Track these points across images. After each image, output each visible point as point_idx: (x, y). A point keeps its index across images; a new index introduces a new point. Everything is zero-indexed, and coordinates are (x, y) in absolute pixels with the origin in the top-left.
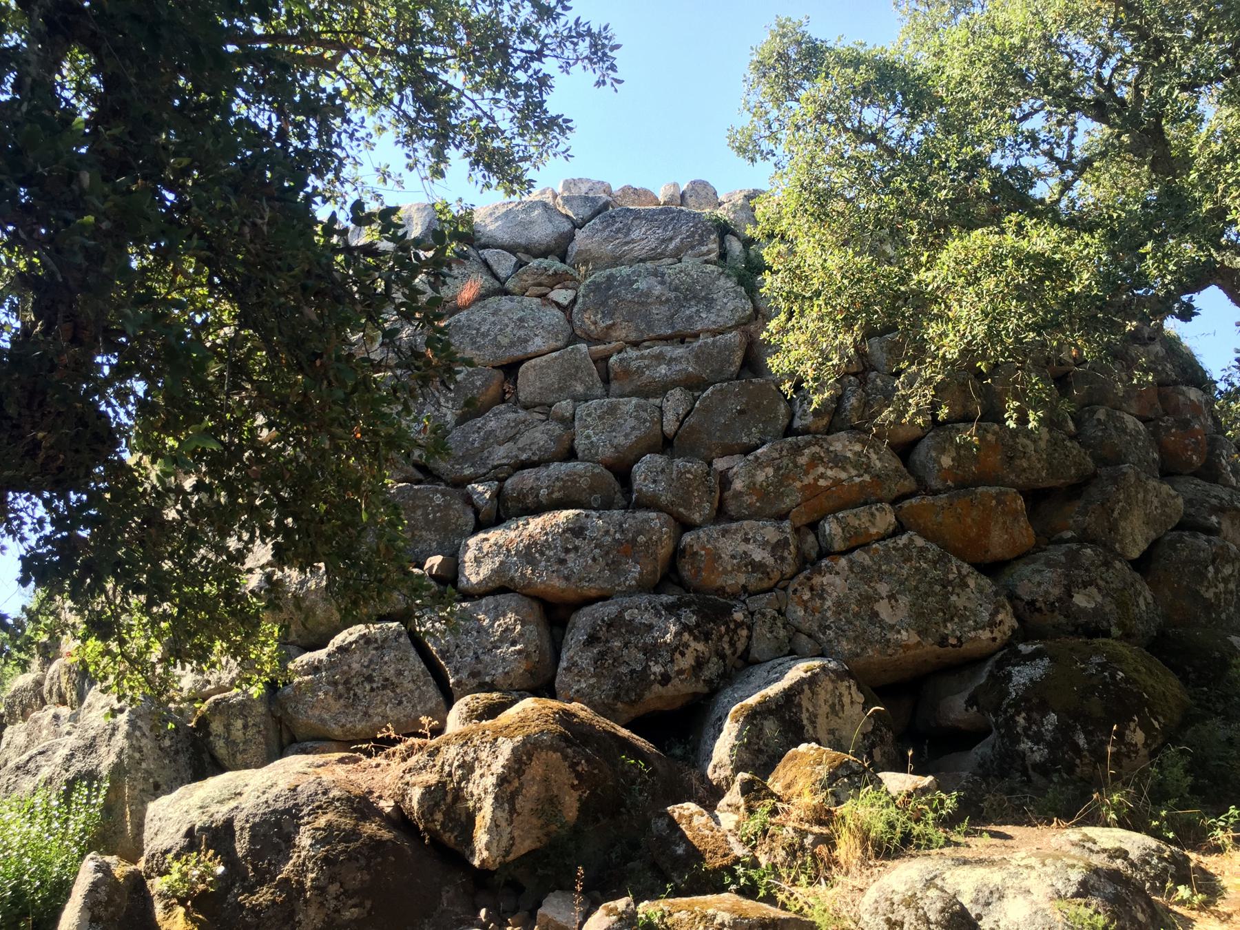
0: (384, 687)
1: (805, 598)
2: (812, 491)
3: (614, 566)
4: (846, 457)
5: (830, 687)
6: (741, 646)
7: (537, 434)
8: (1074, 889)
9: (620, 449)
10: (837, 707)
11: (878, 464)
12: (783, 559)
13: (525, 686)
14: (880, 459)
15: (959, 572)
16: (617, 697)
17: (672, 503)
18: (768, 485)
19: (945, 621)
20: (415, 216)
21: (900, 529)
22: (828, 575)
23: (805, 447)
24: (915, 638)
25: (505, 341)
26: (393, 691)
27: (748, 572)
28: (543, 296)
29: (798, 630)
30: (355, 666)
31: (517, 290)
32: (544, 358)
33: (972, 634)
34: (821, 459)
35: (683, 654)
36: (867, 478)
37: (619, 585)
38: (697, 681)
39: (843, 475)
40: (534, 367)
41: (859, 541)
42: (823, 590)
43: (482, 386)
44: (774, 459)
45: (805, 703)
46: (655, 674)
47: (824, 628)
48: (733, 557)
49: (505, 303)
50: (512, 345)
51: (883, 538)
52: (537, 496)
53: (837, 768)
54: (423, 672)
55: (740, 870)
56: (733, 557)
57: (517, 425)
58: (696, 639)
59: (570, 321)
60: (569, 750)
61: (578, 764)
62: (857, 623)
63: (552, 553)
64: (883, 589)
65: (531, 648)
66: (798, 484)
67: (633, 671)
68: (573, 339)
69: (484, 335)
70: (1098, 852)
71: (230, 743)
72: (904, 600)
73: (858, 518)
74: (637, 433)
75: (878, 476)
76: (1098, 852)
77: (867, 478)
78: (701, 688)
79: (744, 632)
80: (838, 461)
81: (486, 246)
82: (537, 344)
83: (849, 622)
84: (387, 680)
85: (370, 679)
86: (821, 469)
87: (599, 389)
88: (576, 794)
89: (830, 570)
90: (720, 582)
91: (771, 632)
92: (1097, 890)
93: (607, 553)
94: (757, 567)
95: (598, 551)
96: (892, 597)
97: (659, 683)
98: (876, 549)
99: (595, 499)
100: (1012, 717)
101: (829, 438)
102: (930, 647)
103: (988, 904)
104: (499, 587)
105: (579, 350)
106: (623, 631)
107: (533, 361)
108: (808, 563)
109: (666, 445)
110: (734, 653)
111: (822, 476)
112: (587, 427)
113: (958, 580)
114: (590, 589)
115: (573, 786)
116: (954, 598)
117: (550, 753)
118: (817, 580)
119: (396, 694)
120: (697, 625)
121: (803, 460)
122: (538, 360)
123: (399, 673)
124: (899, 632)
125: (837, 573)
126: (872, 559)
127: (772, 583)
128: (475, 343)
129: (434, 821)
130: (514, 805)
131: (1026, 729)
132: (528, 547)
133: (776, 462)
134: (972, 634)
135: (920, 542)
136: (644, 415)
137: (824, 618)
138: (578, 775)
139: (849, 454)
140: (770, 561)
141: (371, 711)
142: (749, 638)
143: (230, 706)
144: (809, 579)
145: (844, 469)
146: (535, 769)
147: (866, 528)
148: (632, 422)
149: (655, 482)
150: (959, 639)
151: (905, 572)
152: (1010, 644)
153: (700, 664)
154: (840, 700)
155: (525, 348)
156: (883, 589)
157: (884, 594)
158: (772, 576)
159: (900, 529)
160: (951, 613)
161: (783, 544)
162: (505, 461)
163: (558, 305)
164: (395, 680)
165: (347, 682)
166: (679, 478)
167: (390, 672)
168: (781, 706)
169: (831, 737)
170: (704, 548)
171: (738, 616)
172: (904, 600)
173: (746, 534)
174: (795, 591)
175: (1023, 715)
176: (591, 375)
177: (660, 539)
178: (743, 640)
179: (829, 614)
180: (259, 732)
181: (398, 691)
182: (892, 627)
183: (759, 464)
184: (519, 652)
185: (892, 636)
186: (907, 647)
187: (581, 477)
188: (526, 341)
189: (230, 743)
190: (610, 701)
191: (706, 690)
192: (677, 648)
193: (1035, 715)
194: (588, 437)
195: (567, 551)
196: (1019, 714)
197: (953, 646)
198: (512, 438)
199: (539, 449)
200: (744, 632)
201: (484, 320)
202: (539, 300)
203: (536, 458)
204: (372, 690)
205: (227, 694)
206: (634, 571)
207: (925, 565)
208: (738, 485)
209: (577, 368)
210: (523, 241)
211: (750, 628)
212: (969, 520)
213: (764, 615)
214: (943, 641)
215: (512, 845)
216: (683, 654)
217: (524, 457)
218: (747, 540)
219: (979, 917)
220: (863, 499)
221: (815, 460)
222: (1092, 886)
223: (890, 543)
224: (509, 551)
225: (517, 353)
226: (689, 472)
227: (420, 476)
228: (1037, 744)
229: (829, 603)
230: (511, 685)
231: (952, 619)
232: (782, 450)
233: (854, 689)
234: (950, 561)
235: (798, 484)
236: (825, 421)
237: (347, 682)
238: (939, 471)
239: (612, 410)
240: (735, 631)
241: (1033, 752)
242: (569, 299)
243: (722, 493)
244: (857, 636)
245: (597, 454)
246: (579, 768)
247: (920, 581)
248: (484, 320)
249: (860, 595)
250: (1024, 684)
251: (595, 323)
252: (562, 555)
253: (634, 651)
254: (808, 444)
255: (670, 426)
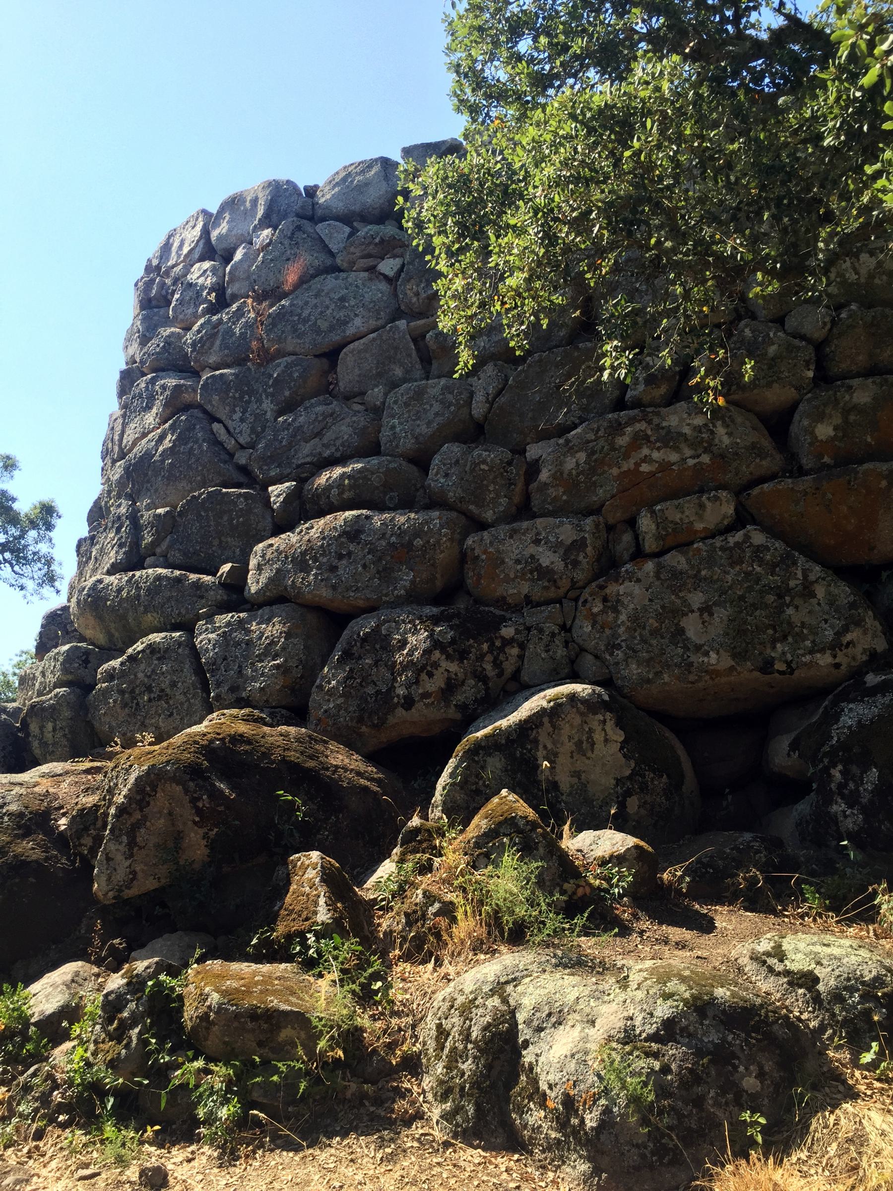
0: (160, 698)
1: (595, 610)
2: (633, 478)
3: (386, 575)
4: (680, 434)
5: (578, 720)
6: (509, 667)
7: (343, 428)
8: (651, 1030)
9: (421, 439)
10: (585, 745)
11: (726, 440)
12: (576, 563)
13: (284, 703)
14: (729, 434)
15: (805, 576)
16: (360, 720)
17: (461, 500)
18: (578, 475)
19: (774, 642)
20: (260, 195)
21: (741, 519)
22: (627, 583)
23: (628, 424)
24: (727, 662)
25: (324, 325)
26: (167, 703)
27: (532, 580)
28: (372, 269)
29: (583, 650)
30: (140, 675)
31: (345, 265)
32: (362, 341)
33: (808, 658)
34: (647, 438)
35: (430, 675)
36: (706, 459)
37: (386, 595)
38: (447, 706)
39: (674, 457)
40: (352, 352)
41: (678, 540)
42: (618, 601)
43: (300, 377)
44: (588, 442)
45: (543, 739)
46: (398, 696)
47: (612, 647)
48: (518, 562)
49: (330, 282)
50: (332, 328)
51: (712, 535)
52: (328, 497)
53: (500, 824)
54: (193, 684)
55: (311, 938)
56: (518, 562)
57: (324, 419)
58: (449, 657)
59: (395, 294)
60: (191, 784)
61: (199, 799)
62: (654, 642)
63: (325, 560)
64: (697, 599)
65: (292, 663)
66: (615, 471)
67: (378, 692)
68: (397, 314)
69: (305, 321)
70: (779, 974)
71: (44, 744)
72: (721, 614)
73: (681, 512)
74: (440, 419)
75: (722, 456)
76: (779, 974)
77: (706, 459)
78: (452, 713)
79: (515, 651)
80: (670, 439)
81: (323, 219)
82: (357, 324)
83: (644, 641)
84: (162, 690)
85: (149, 689)
86: (645, 451)
87: (418, 372)
88: (201, 831)
89: (630, 576)
90: (500, 591)
91: (547, 651)
92: (690, 1035)
93: (380, 559)
94: (545, 574)
95: (370, 556)
96: (706, 609)
97: (402, 706)
98: (699, 550)
99: (391, 498)
100: (826, 770)
101: (664, 411)
102: (748, 674)
103: (540, 1029)
104: (277, 598)
105: (397, 327)
106: (378, 646)
107: (351, 346)
108: (608, 566)
109: (474, 432)
110: (500, 675)
111: (646, 459)
112: (393, 417)
113: (800, 588)
114: (357, 599)
115: (195, 823)
116: (790, 611)
117: (174, 785)
118: (612, 589)
119: (170, 706)
120: (453, 641)
121: (622, 441)
122: (356, 343)
123: (173, 684)
124: (707, 654)
125: (638, 580)
126: (688, 561)
127: (562, 591)
128: (296, 330)
129: (81, 845)
130: (135, 837)
131: (841, 786)
132: (304, 554)
133: (591, 445)
134: (808, 658)
135: (758, 538)
136: (450, 397)
137: (615, 635)
138: (199, 812)
139: (686, 430)
140: (559, 566)
141: (147, 721)
142: (521, 657)
143: (43, 709)
144: (602, 587)
145: (676, 449)
146: (161, 801)
147: (691, 523)
148: (437, 407)
149: (446, 475)
150: (789, 664)
151: (729, 578)
152: (857, 674)
153: (451, 686)
154: (590, 737)
155: (344, 331)
156: (697, 599)
157: (695, 606)
158: (560, 583)
159: (741, 519)
160: (785, 632)
161: (579, 545)
162: (308, 459)
163: (386, 277)
164: (168, 691)
165: (133, 691)
166: (473, 470)
167: (165, 684)
168: (513, 741)
169: (575, 780)
170: (485, 552)
171: (507, 631)
172: (721, 614)
173: (538, 534)
174: (586, 601)
175: (840, 767)
176: (409, 355)
177: (438, 542)
178: (512, 660)
179: (622, 630)
180: (65, 735)
181: (171, 702)
182: (698, 648)
183: (570, 449)
184: (277, 667)
185: (697, 659)
186: (714, 673)
187: (373, 473)
188: (346, 323)
189: (44, 744)
190: (354, 724)
191: (458, 716)
192: (424, 667)
193: (855, 770)
194: (393, 427)
195: (340, 557)
196: (835, 767)
197: (781, 673)
198: (319, 434)
199: (343, 445)
200: (515, 651)
201: (306, 303)
202: (366, 274)
203: (338, 455)
204: (150, 700)
205: (44, 698)
206: (406, 578)
207: (758, 569)
208: (544, 475)
209: (396, 348)
210: (357, 208)
211: (522, 646)
212: (845, 509)
213: (541, 631)
214: (767, 667)
215: (132, 880)
216: (430, 675)
217: (327, 453)
218: (537, 542)
219: (526, 1044)
220: (698, 485)
221: (640, 440)
222: (682, 1030)
223: (718, 542)
224: (286, 557)
225: (335, 337)
226: (484, 462)
227: (242, 479)
228: (851, 806)
229: (623, 617)
230: (267, 701)
231: (785, 638)
232: (598, 430)
233: (610, 725)
234: (795, 563)
235: (615, 471)
236: (663, 390)
237: (133, 691)
238: (810, 444)
239: (419, 394)
240: (501, 649)
241: (846, 817)
242: (395, 269)
243: (527, 483)
244: (651, 659)
245: (397, 446)
246: (201, 805)
247: (750, 589)
248: (306, 303)
249: (663, 607)
250: (850, 727)
251: (417, 294)
252: (335, 562)
253: (383, 670)
254: (632, 421)
255: (478, 409)
